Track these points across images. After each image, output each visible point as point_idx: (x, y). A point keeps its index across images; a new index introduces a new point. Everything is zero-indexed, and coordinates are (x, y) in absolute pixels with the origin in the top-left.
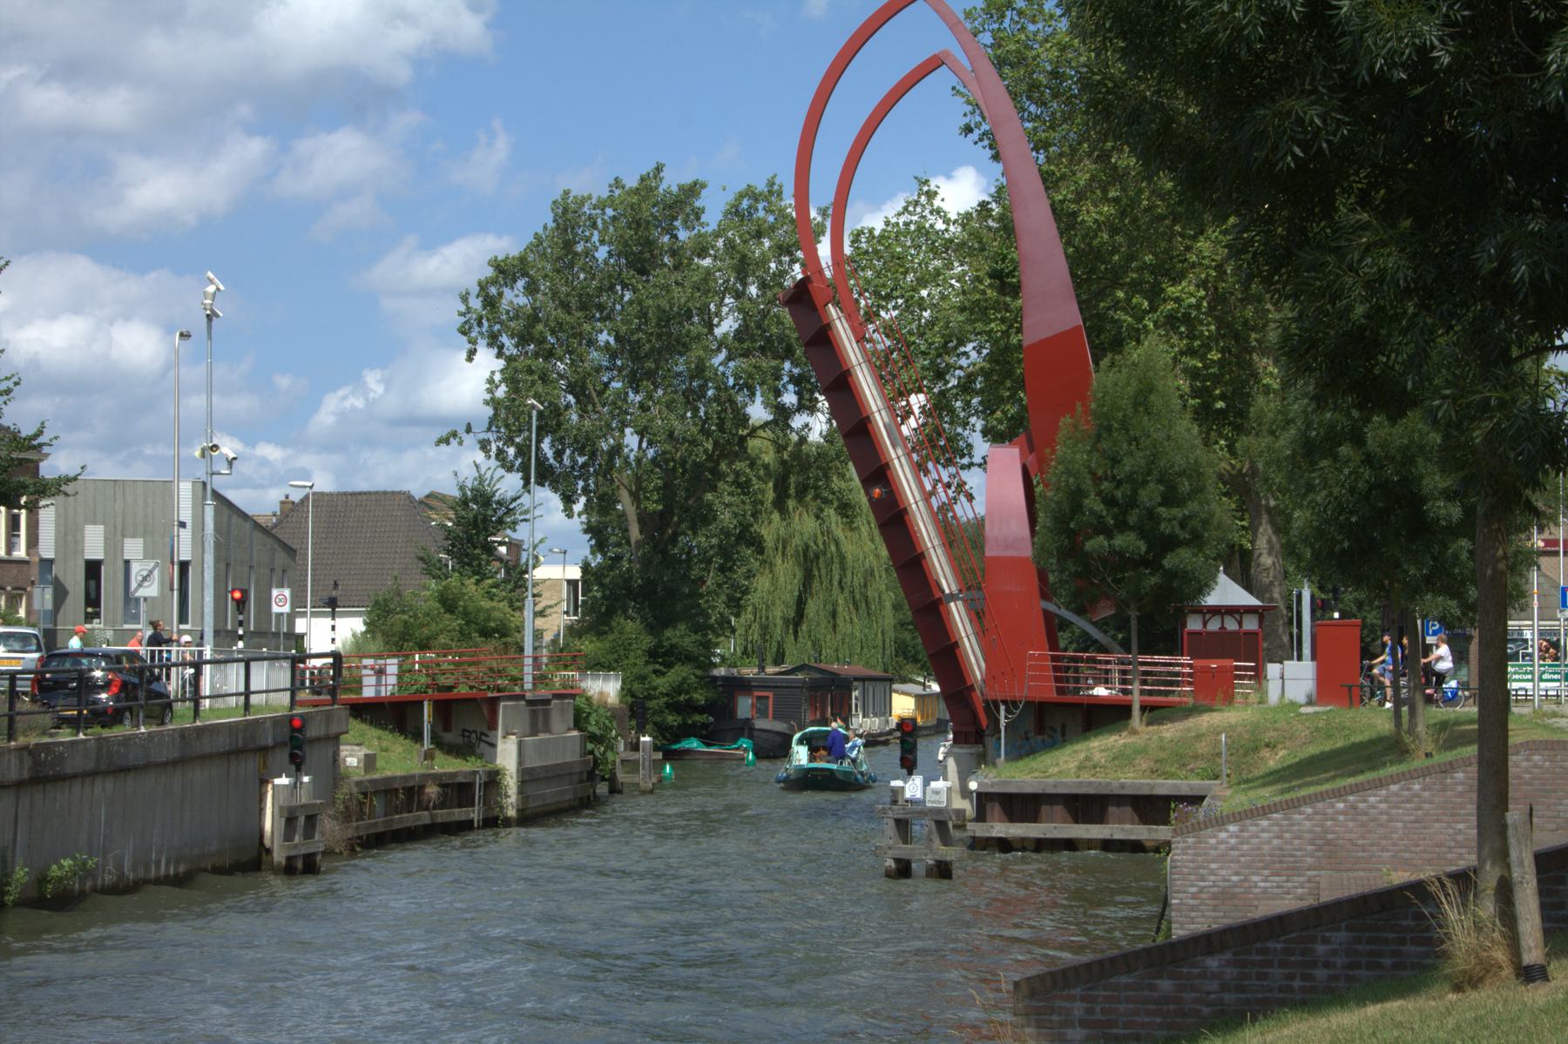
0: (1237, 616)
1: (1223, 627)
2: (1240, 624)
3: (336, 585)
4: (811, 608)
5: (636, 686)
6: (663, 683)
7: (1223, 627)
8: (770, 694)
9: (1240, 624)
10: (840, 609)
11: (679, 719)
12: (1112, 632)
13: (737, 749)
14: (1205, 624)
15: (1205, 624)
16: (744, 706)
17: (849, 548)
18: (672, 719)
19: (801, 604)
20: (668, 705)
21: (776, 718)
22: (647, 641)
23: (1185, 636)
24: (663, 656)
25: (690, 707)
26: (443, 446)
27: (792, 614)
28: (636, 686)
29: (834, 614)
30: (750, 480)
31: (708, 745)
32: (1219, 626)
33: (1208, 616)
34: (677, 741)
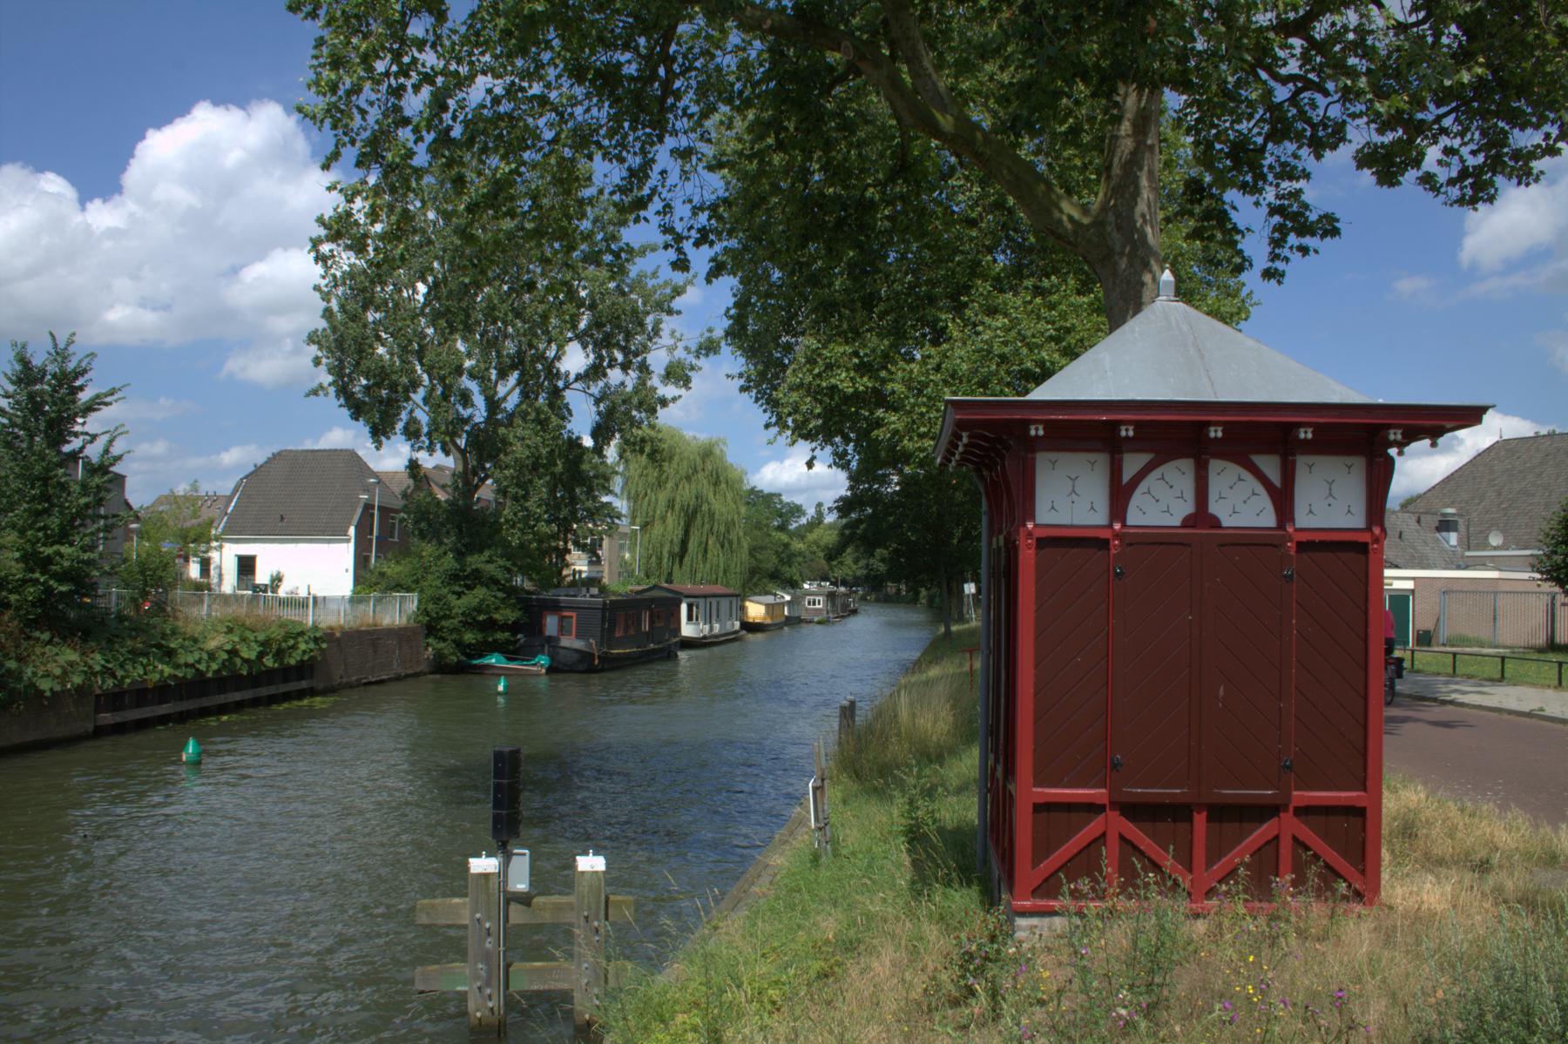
0: (1270, 465)
1: (1201, 517)
2: (1283, 499)
3: (282, 518)
4: (692, 545)
5: (431, 606)
6: (460, 604)
7: (1201, 517)
8: (573, 614)
9: (1283, 499)
10: (710, 547)
11: (480, 636)
12: (335, 227)
13: (535, 665)
14: (1120, 496)
15: (1120, 496)
16: (551, 624)
17: (717, 506)
18: (469, 637)
19: (684, 544)
20: (465, 623)
21: (578, 636)
22: (449, 562)
23: (1027, 555)
24: (464, 579)
25: (491, 625)
26: (312, 397)
27: (677, 549)
28: (431, 606)
29: (706, 551)
30: (549, 418)
31: (510, 659)
32: (1186, 508)
33: (1132, 464)
34: (481, 656)
